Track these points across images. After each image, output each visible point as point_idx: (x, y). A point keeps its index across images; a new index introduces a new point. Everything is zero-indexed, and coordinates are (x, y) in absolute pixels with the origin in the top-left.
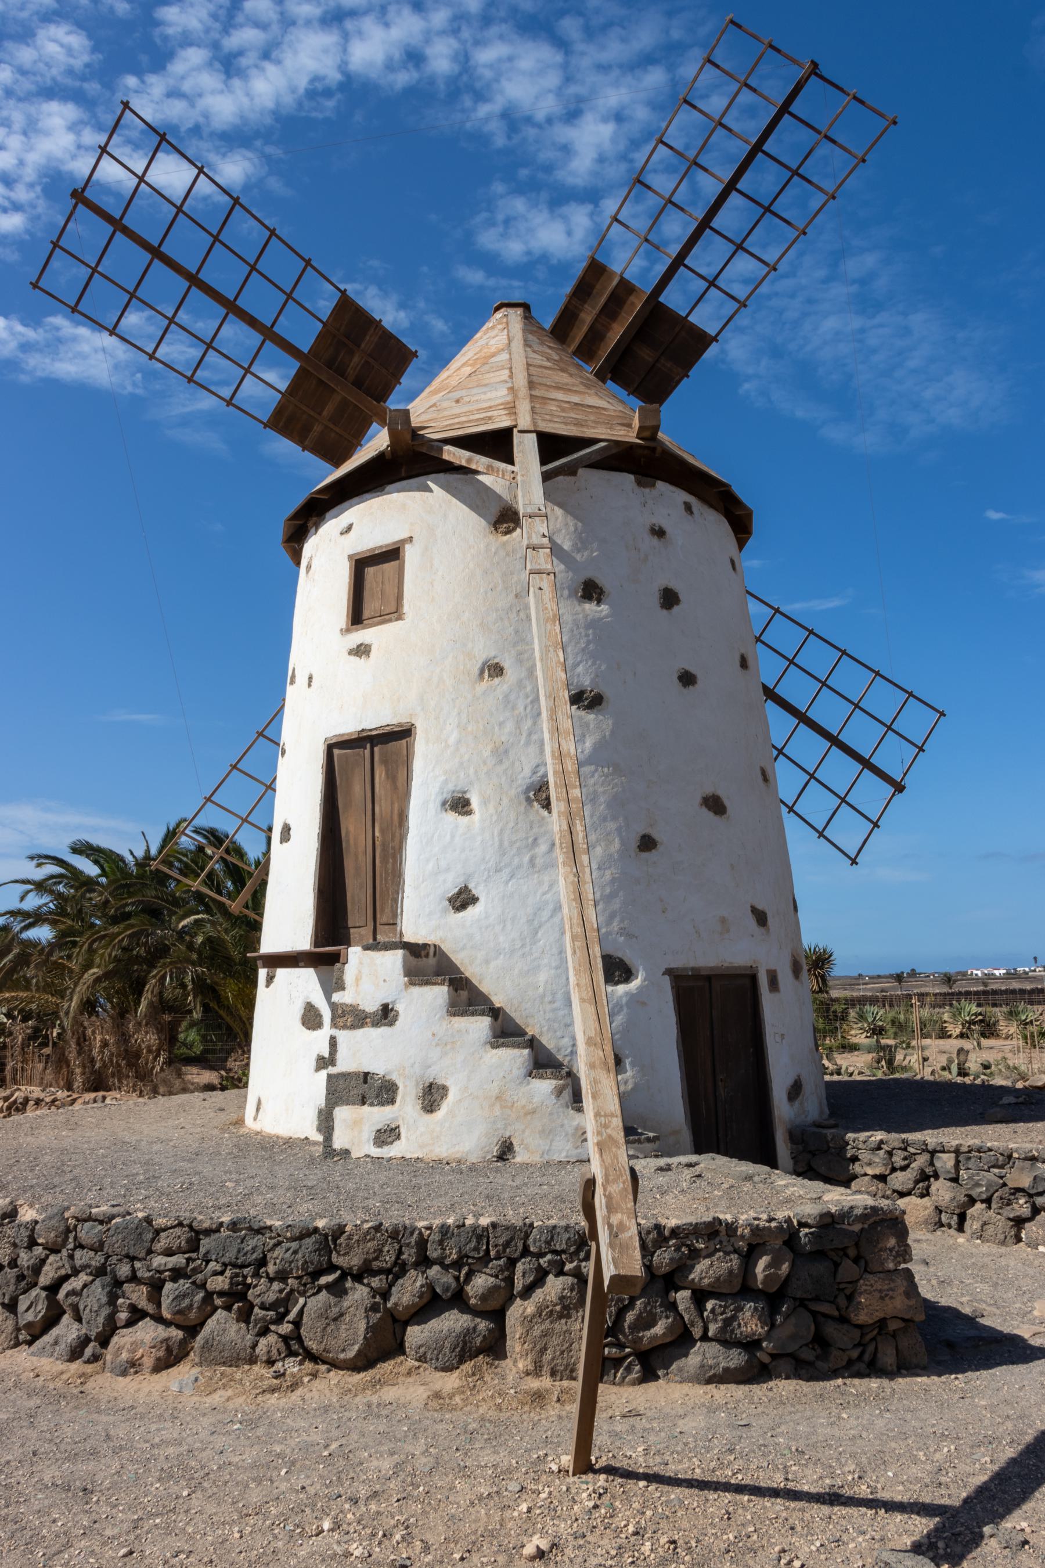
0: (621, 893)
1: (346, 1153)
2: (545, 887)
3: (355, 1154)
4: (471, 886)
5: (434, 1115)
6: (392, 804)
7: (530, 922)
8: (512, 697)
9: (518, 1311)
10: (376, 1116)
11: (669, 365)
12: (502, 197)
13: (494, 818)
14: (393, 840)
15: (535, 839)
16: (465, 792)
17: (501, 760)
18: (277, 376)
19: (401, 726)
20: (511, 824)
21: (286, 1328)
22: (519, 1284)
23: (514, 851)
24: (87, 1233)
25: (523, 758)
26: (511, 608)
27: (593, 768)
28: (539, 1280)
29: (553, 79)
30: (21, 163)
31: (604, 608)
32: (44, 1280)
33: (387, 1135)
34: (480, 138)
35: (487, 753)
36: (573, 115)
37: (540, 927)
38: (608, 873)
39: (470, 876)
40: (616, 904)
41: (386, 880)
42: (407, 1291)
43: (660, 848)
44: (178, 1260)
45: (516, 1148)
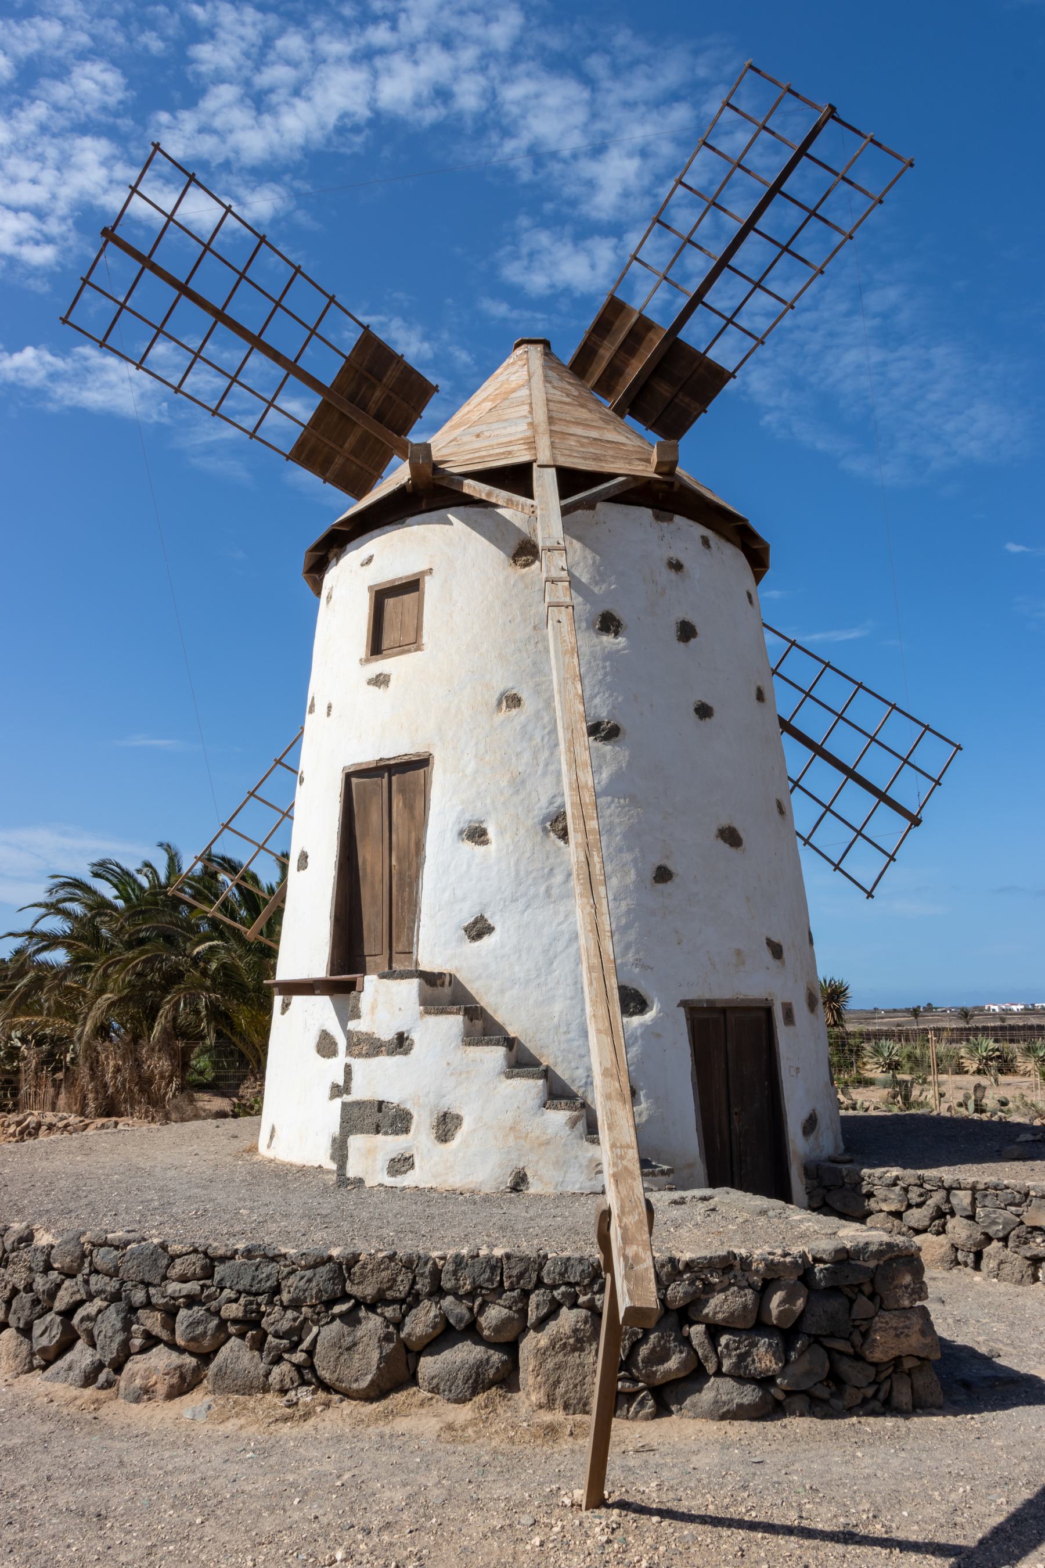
1: (360, 1181)
2: (561, 917)
3: (368, 1183)
4: (486, 916)
5: (448, 1144)
6: (409, 832)
7: (545, 952)
8: (530, 728)
9: (531, 1344)
10: (390, 1145)
11: (687, 400)
12: (526, 230)
13: (511, 848)
14: (409, 868)
15: (552, 870)
16: (482, 822)
18: (301, 406)
19: (419, 756)
20: (528, 854)
21: (299, 1357)
22: (532, 1316)
23: (530, 881)
24: (103, 1258)
25: (540, 789)
26: (529, 639)
27: (609, 798)
28: (553, 1313)
29: (579, 116)
30: (54, 197)
31: (621, 640)
32: (60, 1304)
33: (401, 1164)
34: (507, 173)
35: (504, 783)
36: (598, 151)
38: (623, 904)
40: (632, 935)
41: (402, 908)
42: (421, 1321)
43: (676, 880)
44: (193, 1287)
45: (530, 1179)
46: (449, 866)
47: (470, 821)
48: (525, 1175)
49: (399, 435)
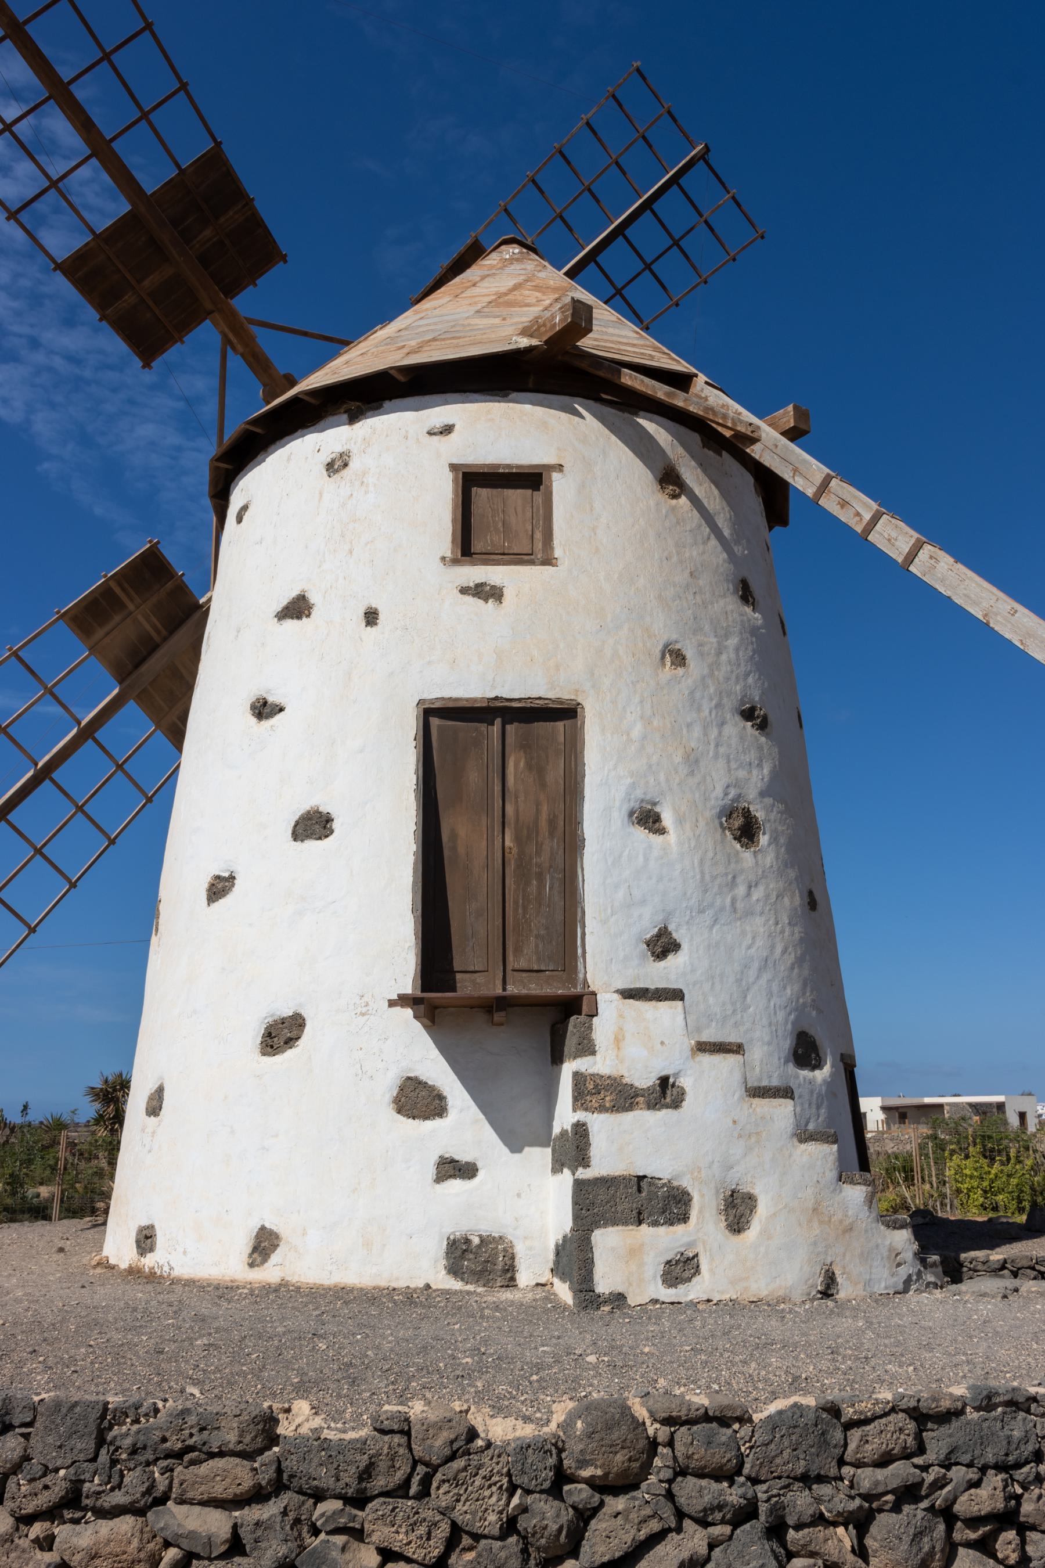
0: (808, 958)
1: (618, 1299)
3: (632, 1301)
4: (671, 928)
5: (743, 1236)
7: (739, 981)
8: (698, 695)
10: (660, 1241)
13: (693, 844)
14: (538, 853)
15: (734, 877)
16: (655, 804)
17: (693, 771)
18: (107, 207)
19: (562, 703)
20: (710, 854)
25: (713, 774)
26: (688, 586)
33: (681, 1268)
35: (678, 759)
37: (748, 989)
39: (669, 915)
41: (525, 908)
44: (900, 1472)
45: (839, 1280)
46: (620, 856)
47: (642, 801)
48: (833, 1273)
49: (226, 297)
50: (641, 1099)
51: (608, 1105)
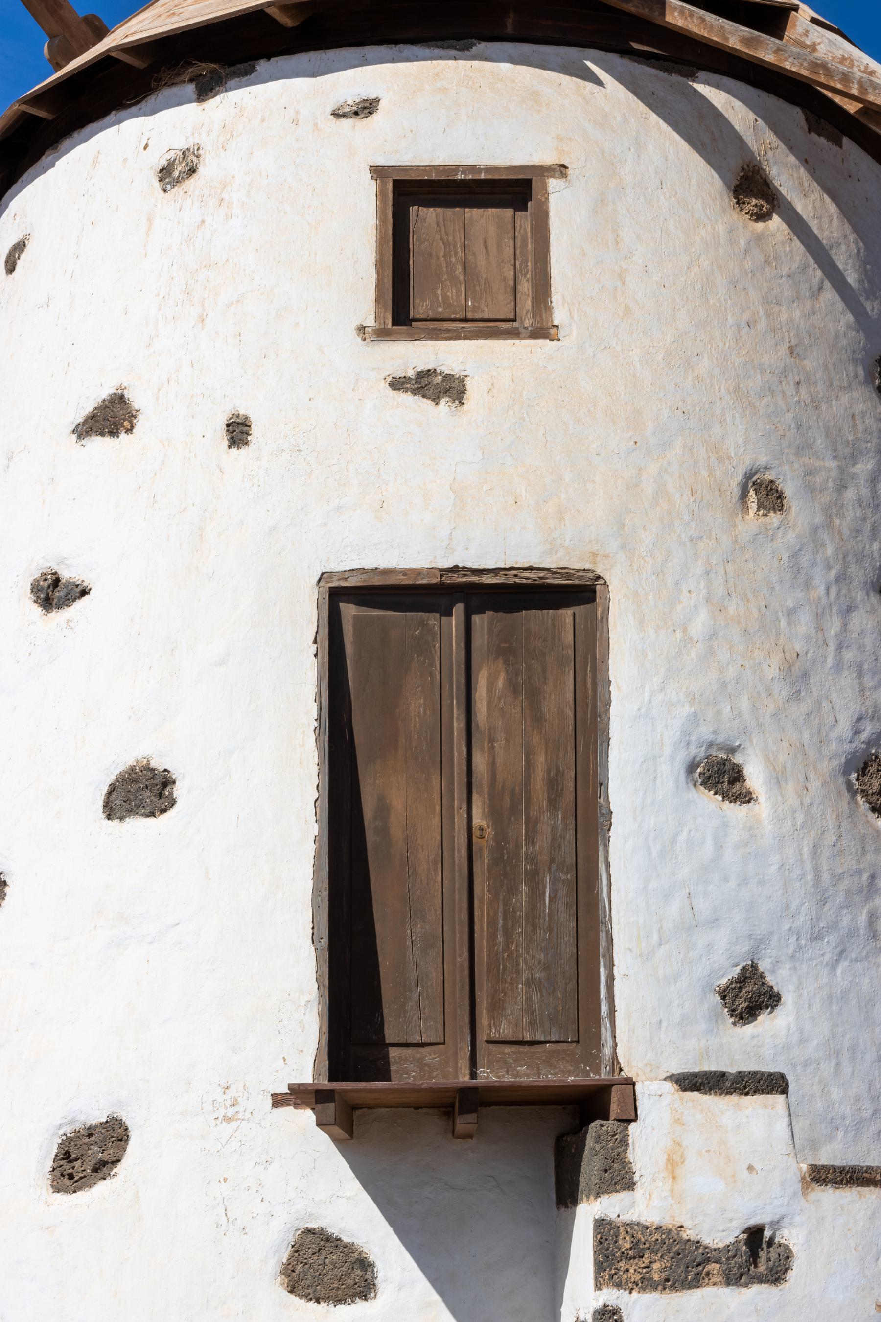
4: (764, 966)
6: (529, 752)
8: (805, 560)
13: (800, 818)
14: (530, 837)
16: (733, 750)
19: (568, 576)
20: (830, 838)
23: (840, 898)
25: (834, 697)
35: (772, 672)
46: (673, 842)
47: (711, 745)
50: (714, 1267)
51: (656, 1277)
